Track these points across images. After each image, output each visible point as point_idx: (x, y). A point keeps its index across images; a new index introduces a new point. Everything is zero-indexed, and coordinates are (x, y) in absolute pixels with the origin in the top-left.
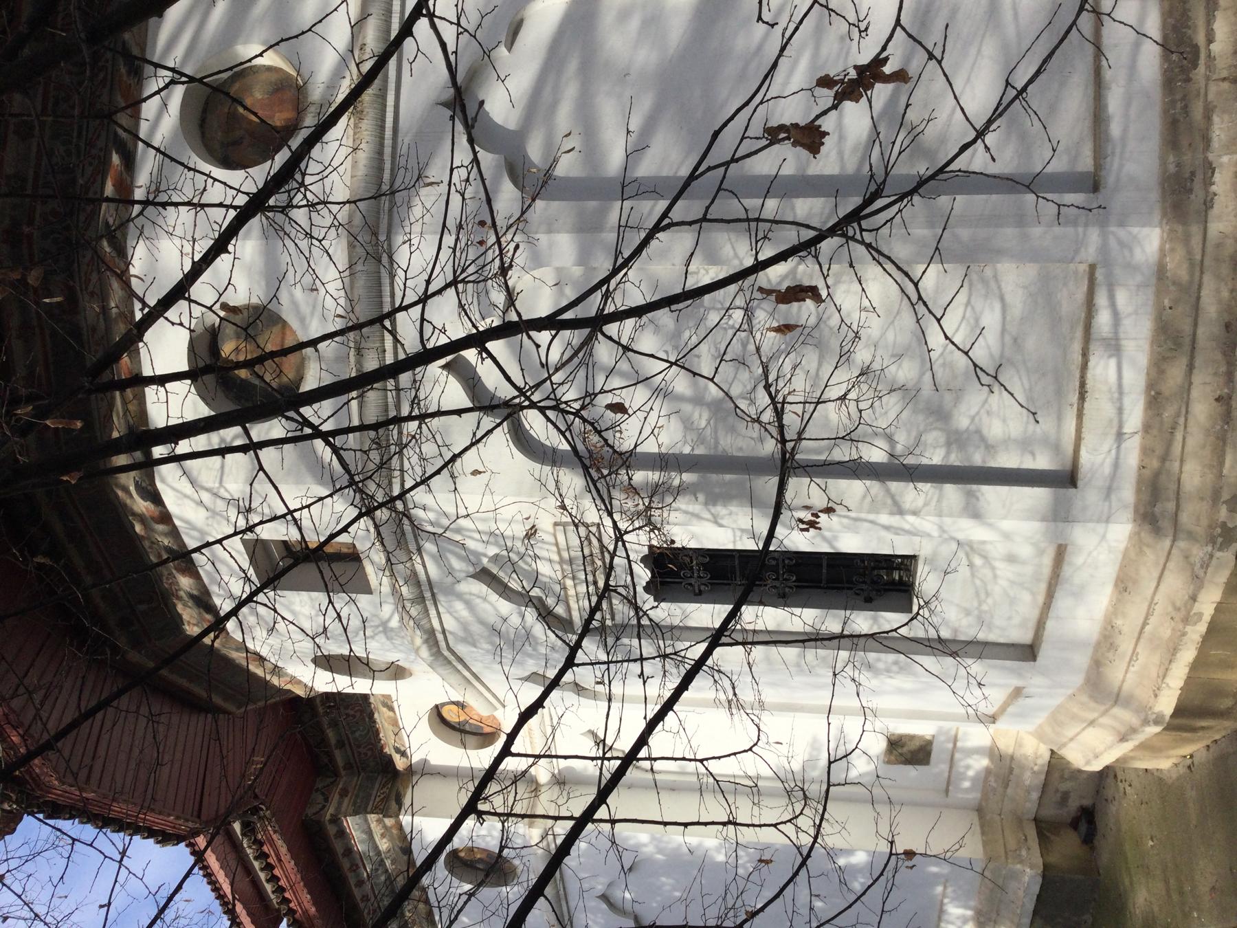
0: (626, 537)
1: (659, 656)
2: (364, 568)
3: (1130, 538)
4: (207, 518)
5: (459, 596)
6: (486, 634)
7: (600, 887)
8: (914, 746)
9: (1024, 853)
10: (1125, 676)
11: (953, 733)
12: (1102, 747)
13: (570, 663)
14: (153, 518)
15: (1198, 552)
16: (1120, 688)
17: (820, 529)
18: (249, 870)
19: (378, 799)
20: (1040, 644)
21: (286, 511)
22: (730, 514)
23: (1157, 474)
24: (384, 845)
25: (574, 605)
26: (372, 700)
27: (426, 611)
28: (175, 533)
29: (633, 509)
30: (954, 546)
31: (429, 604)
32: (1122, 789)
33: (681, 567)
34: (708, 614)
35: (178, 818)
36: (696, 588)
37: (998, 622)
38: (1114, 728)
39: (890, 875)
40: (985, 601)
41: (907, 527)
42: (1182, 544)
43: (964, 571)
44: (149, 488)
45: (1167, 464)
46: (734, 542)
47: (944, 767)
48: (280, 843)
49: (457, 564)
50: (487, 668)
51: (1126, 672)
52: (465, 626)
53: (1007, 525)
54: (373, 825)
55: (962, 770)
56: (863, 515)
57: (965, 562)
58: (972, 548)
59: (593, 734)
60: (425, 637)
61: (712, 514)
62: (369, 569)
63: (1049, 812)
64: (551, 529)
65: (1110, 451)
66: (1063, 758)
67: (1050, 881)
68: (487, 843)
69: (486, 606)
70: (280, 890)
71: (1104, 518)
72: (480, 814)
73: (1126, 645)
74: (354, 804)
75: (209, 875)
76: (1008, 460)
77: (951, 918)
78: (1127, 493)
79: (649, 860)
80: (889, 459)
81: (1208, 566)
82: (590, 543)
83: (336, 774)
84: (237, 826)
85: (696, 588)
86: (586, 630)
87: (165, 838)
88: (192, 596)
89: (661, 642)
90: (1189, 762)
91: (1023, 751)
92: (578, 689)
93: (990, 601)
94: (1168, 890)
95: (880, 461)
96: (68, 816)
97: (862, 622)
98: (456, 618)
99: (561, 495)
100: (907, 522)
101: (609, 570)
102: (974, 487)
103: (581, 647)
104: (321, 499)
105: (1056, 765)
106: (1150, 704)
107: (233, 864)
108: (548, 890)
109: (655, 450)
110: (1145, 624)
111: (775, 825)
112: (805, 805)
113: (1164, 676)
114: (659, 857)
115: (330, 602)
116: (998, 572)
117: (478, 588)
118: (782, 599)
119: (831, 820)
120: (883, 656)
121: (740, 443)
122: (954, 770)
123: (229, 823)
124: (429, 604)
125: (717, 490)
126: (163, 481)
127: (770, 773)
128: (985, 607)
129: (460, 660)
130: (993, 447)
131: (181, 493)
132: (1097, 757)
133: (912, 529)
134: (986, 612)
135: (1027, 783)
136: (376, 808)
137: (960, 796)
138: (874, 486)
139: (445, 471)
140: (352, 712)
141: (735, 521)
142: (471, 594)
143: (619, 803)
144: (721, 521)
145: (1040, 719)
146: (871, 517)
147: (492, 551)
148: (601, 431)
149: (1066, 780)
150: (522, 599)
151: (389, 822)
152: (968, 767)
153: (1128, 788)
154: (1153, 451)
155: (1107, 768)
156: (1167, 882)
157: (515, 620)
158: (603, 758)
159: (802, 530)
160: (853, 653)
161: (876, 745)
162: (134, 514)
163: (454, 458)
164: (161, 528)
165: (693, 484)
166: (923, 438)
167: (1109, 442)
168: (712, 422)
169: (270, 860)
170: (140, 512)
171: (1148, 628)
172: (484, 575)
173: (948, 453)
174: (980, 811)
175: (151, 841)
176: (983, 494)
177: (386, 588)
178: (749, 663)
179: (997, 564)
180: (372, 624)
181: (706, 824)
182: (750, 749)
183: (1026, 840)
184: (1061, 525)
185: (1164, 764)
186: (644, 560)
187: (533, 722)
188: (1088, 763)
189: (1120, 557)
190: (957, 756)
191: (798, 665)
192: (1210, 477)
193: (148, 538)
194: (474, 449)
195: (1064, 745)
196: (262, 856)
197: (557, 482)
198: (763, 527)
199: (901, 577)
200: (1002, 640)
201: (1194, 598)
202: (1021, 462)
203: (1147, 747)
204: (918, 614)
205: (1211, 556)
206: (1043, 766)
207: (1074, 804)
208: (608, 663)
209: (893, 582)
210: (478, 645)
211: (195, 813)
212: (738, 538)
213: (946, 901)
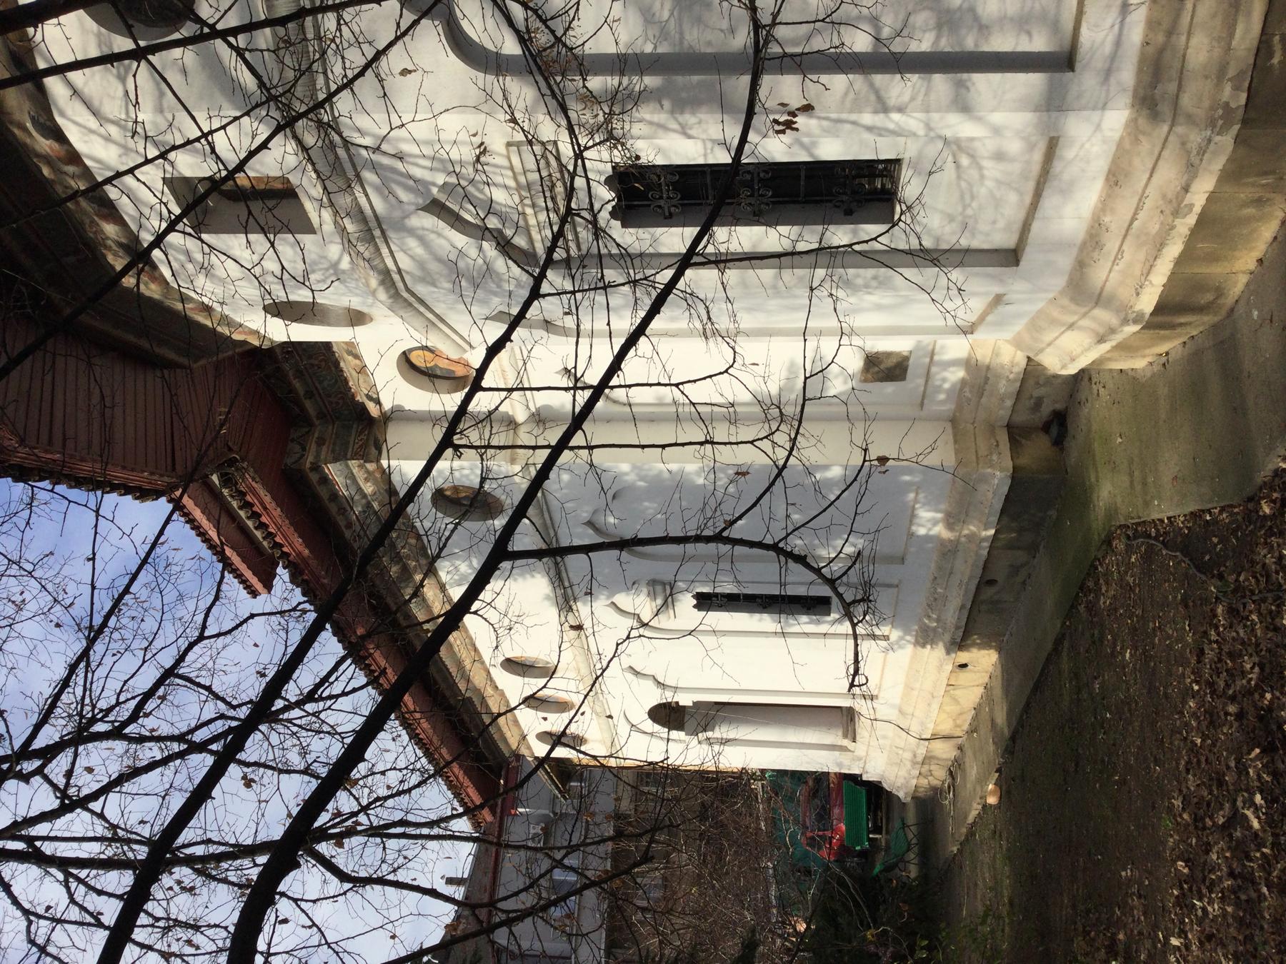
0: (586, 154)
1: (629, 282)
2: (302, 205)
3: (1127, 125)
4: (120, 156)
5: (411, 232)
6: (445, 272)
7: (585, 515)
8: (890, 363)
9: (995, 457)
10: (1108, 276)
11: (931, 347)
12: (1079, 350)
13: (535, 294)
14: (59, 159)
15: (1196, 138)
16: (1102, 289)
17: (797, 130)
18: (233, 517)
19: (356, 446)
20: (1024, 249)
21: (200, 134)
22: (700, 122)
23: (1161, 51)
24: (369, 488)
25: (536, 236)
26: (335, 349)
27: (378, 249)
28: (87, 172)
29: (592, 121)
30: (940, 145)
31: (380, 242)
32: (1095, 392)
33: (649, 187)
34: (676, 239)
35: (152, 474)
36: (666, 210)
37: (983, 227)
38: (1093, 330)
39: (864, 480)
40: (969, 205)
41: (891, 126)
42: (1179, 129)
43: (949, 172)
44: (48, 123)
45: (1174, 38)
46: (705, 155)
47: (921, 381)
48: (262, 492)
49: (403, 195)
50: (451, 308)
51: (1110, 272)
52: (421, 264)
53: (998, 118)
54: (355, 471)
55: (938, 383)
56: (844, 116)
57: (950, 159)
58: (960, 148)
59: (567, 371)
60: (381, 277)
61: (680, 124)
62: (309, 206)
63: (1022, 418)
64: (504, 151)
65: (1113, 26)
66: (1039, 365)
67: (1018, 481)
68: (471, 481)
69: (442, 242)
70: (270, 536)
71: (1100, 105)
72: (457, 448)
73: (1112, 244)
74: (333, 451)
75: (191, 521)
76: (1002, 43)
77: (922, 521)
78: (1127, 75)
79: (631, 488)
80: (875, 46)
81: (1205, 152)
82: (548, 163)
83: (311, 425)
84: (215, 478)
85: (666, 210)
86: (549, 262)
87: (143, 494)
88: (121, 245)
89: (631, 272)
90: (1164, 359)
91: (998, 361)
92: (547, 325)
93: (974, 204)
94: (1132, 482)
95: (864, 50)
96: (37, 478)
97: (840, 235)
98: (411, 257)
99: (510, 106)
100: (892, 121)
101: (570, 192)
102: (965, 76)
103: (545, 277)
104: (236, 119)
105: (1033, 371)
106: (1131, 303)
107: (216, 512)
108: (531, 511)
109: (612, 49)
110: (1133, 219)
111: (752, 442)
112: (782, 421)
113: (1148, 273)
114: (641, 484)
115: (250, 213)
116: (986, 172)
117: (428, 221)
118: (756, 217)
119: (807, 435)
120: (861, 271)
121: (709, 36)
122: (930, 383)
123: (207, 476)
124: (380, 242)
125: (684, 95)
126: (62, 114)
127: (747, 397)
128: (969, 212)
129: (421, 302)
130: (987, 27)
131: (85, 127)
132: (1073, 360)
133: (897, 129)
134: (970, 217)
135: (1002, 391)
136: (356, 454)
137: (935, 408)
138: (858, 80)
139: (369, 73)
140: (316, 362)
141: (705, 131)
142: (423, 229)
143: (593, 431)
144: (691, 132)
145: (1019, 326)
146: (853, 117)
147: (440, 179)
148: (547, 20)
149: (1041, 386)
150: (480, 232)
151: (371, 467)
152: (944, 380)
153: (1102, 390)
154: (1160, 24)
155: (1082, 371)
156: (1131, 475)
157: (473, 252)
158: (575, 388)
159: (778, 132)
160: (830, 270)
161: (854, 363)
162: (38, 155)
163: (379, 55)
164: (70, 169)
165: (658, 89)
166: (911, 19)
167: (1112, 17)
168: (675, 13)
169: (255, 509)
170: (44, 153)
171: (1136, 223)
172: (436, 208)
173: (938, 38)
174: (953, 421)
175: (129, 497)
176: (974, 84)
177: (328, 227)
178: (723, 283)
179: (985, 163)
180: (321, 266)
181: (683, 445)
182: (726, 371)
183: (997, 445)
184: (1054, 114)
185: (1139, 363)
186: (609, 182)
187: (503, 355)
188: (1064, 367)
189: (1114, 148)
190: (934, 369)
191: (775, 287)
192: (1217, 52)
193: (61, 184)
194: (400, 43)
195: (1042, 351)
196: (246, 505)
197: (504, 91)
198: (734, 133)
199: (883, 185)
200: (986, 246)
201: (1186, 189)
202: (1017, 44)
203: (1125, 348)
204: (900, 220)
205: (1209, 141)
206: (1019, 373)
207: (1046, 410)
208: (573, 293)
209: (874, 191)
210: (439, 285)
211: (169, 468)
212: (709, 151)
213: (917, 506)
